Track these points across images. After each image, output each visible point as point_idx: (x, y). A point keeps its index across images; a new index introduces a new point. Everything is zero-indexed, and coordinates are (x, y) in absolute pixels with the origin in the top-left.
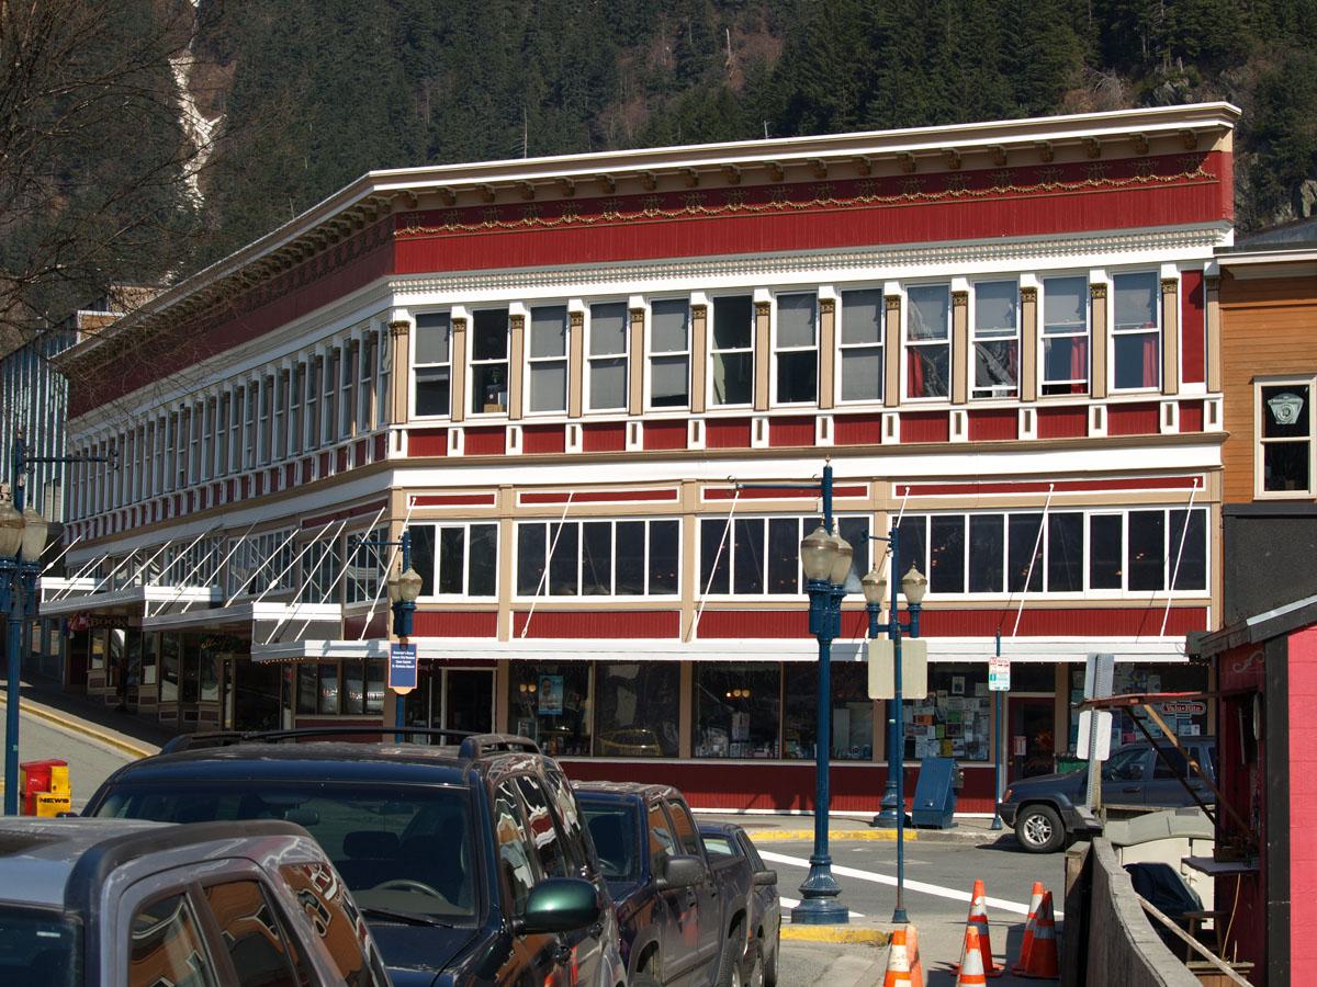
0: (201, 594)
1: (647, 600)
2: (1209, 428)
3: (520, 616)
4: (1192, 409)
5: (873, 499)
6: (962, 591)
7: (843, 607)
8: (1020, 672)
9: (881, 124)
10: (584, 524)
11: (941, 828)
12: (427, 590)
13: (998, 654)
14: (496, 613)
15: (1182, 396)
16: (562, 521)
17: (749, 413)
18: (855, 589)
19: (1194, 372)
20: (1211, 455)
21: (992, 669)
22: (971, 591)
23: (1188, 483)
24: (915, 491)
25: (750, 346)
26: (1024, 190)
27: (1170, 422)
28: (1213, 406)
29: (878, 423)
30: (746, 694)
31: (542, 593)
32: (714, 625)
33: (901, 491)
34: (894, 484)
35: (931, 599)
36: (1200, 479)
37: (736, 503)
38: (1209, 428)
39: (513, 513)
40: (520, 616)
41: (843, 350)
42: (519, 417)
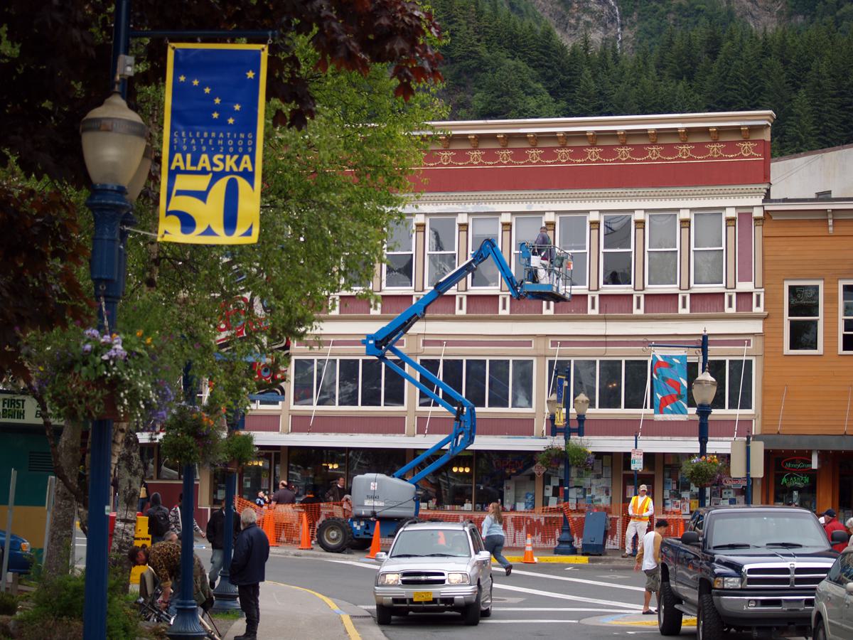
0: (205, 401)
1: (383, 409)
2: (756, 310)
3: (422, 420)
4: (744, 296)
5: (536, 349)
6: (380, 405)
7: (710, 418)
8: (649, 458)
9: (582, 111)
10: (340, 360)
11: (600, 555)
12: (592, 405)
13: (636, 447)
14: (278, 416)
15: (693, 291)
16: (556, 359)
17: (586, 292)
18: (522, 405)
19: (745, 277)
20: (757, 327)
21: (633, 456)
22: (600, 407)
23: (741, 343)
24: (563, 344)
25: (630, 248)
26: (548, 161)
27: (593, 307)
28: (758, 297)
29: (792, 302)
30: (467, 470)
31: (646, 407)
32: (300, 423)
33: (554, 344)
34: (551, 339)
35: (596, 412)
36: (749, 341)
37: (443, 349)
38: (756, 310)
39: (548, 354)
40: (422, 420)
41: (694, 251)
42: (464, 289)
